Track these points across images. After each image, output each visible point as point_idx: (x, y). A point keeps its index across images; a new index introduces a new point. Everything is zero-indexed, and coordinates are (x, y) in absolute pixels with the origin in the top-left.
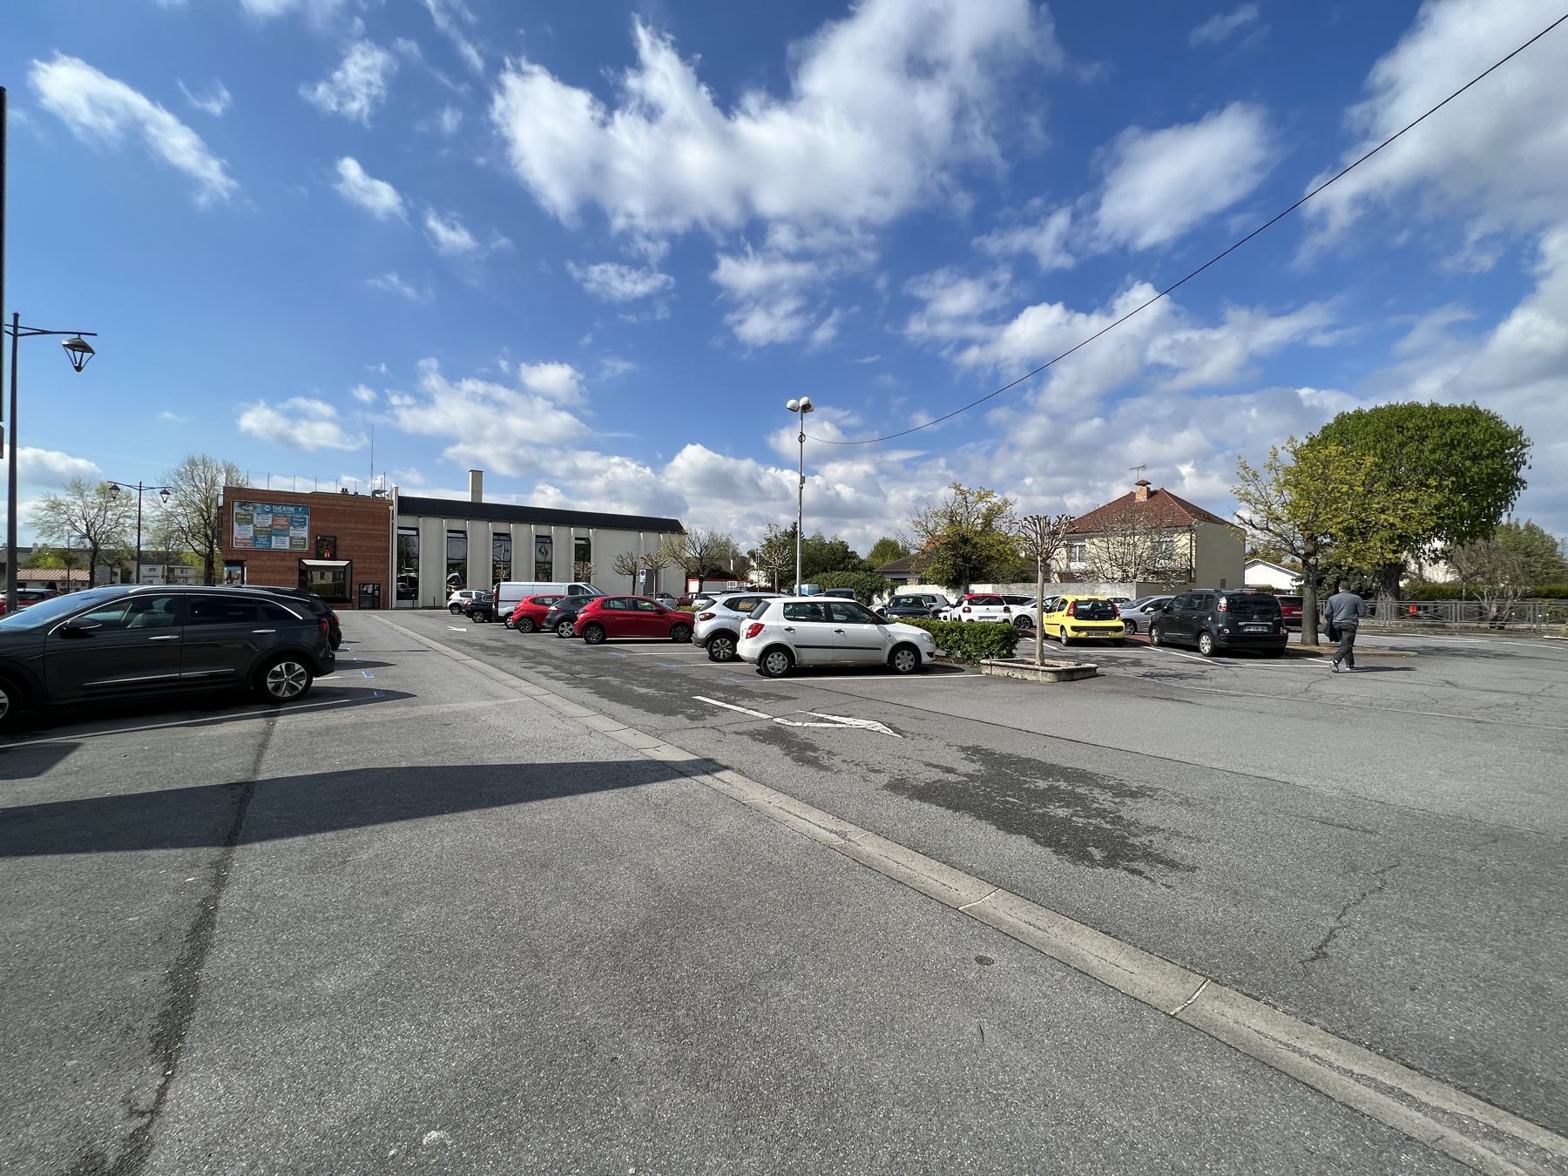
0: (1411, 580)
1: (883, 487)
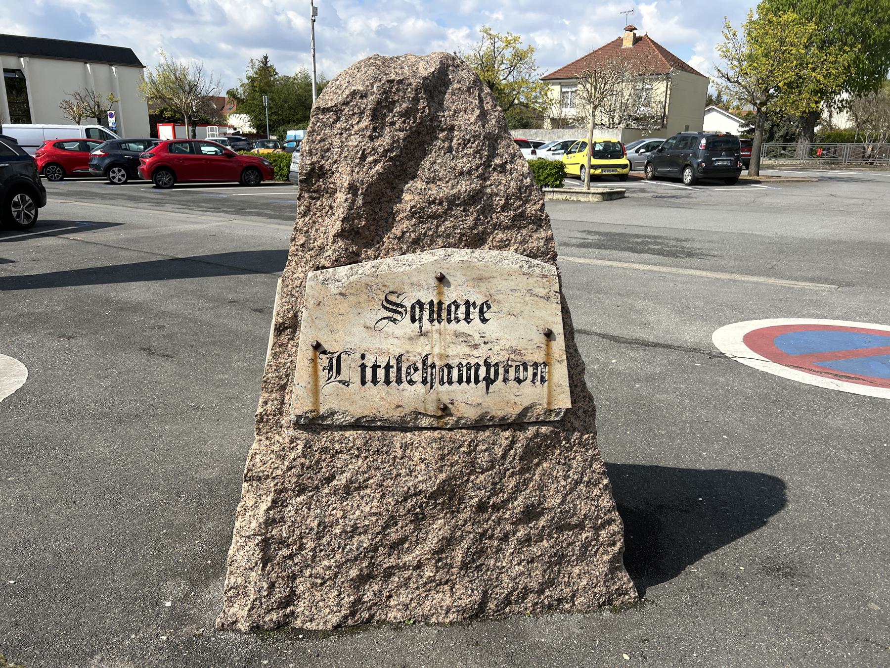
0: (823, 126)
1: (342, 14)
